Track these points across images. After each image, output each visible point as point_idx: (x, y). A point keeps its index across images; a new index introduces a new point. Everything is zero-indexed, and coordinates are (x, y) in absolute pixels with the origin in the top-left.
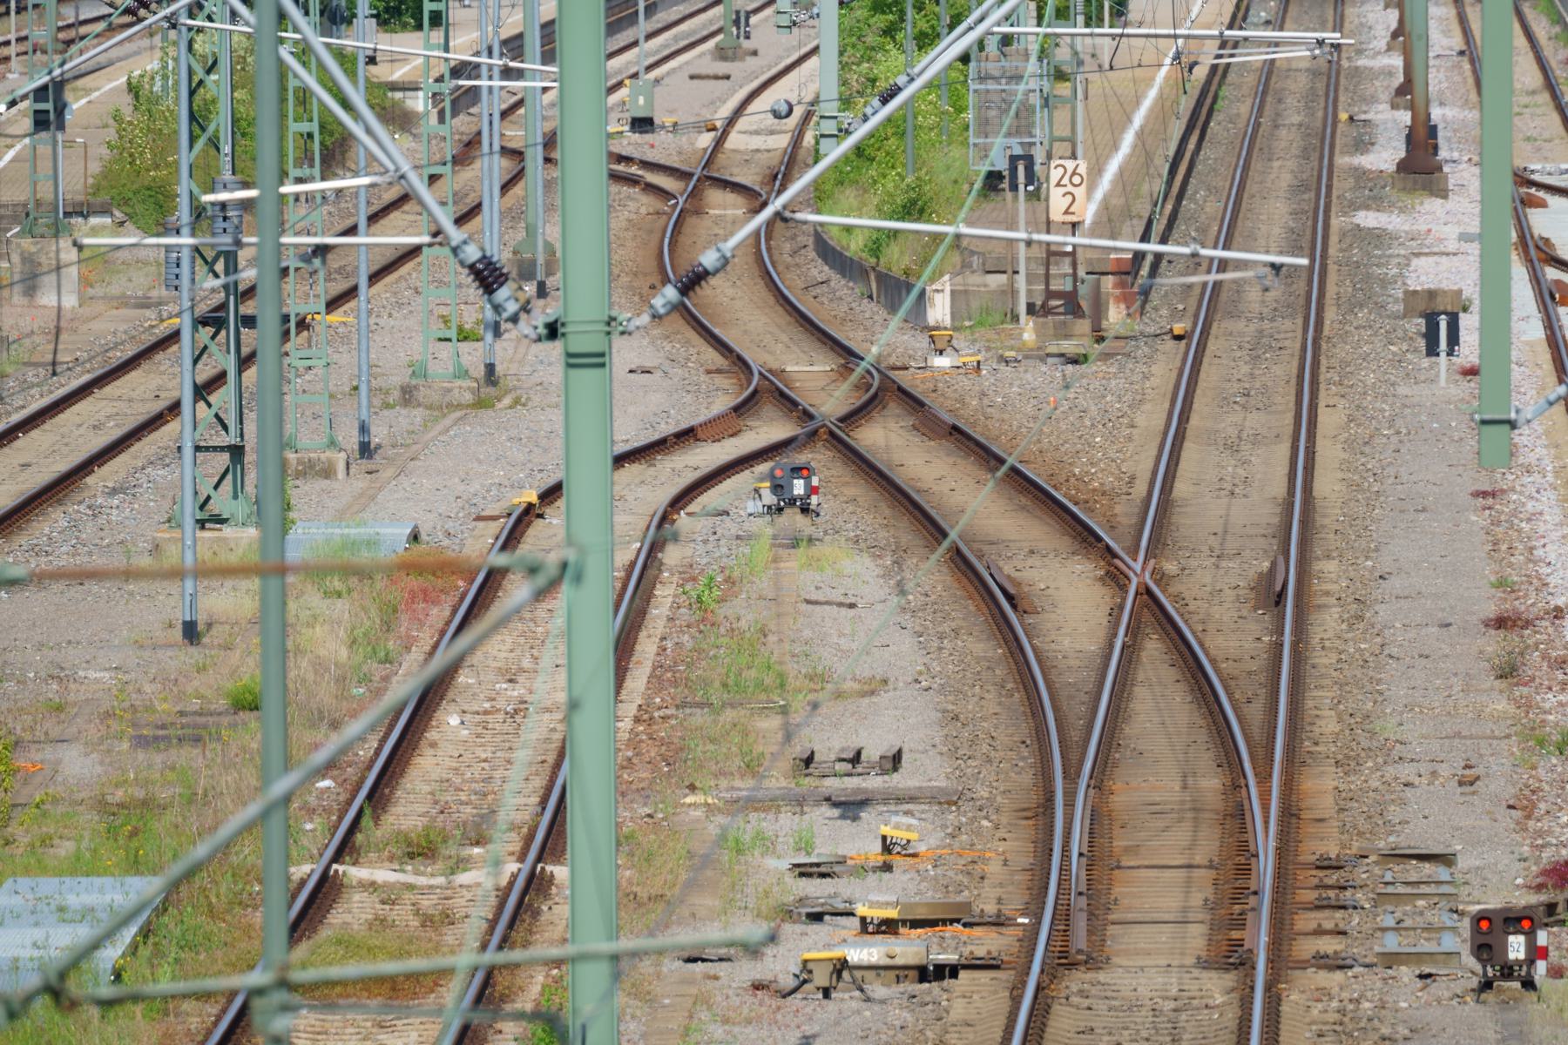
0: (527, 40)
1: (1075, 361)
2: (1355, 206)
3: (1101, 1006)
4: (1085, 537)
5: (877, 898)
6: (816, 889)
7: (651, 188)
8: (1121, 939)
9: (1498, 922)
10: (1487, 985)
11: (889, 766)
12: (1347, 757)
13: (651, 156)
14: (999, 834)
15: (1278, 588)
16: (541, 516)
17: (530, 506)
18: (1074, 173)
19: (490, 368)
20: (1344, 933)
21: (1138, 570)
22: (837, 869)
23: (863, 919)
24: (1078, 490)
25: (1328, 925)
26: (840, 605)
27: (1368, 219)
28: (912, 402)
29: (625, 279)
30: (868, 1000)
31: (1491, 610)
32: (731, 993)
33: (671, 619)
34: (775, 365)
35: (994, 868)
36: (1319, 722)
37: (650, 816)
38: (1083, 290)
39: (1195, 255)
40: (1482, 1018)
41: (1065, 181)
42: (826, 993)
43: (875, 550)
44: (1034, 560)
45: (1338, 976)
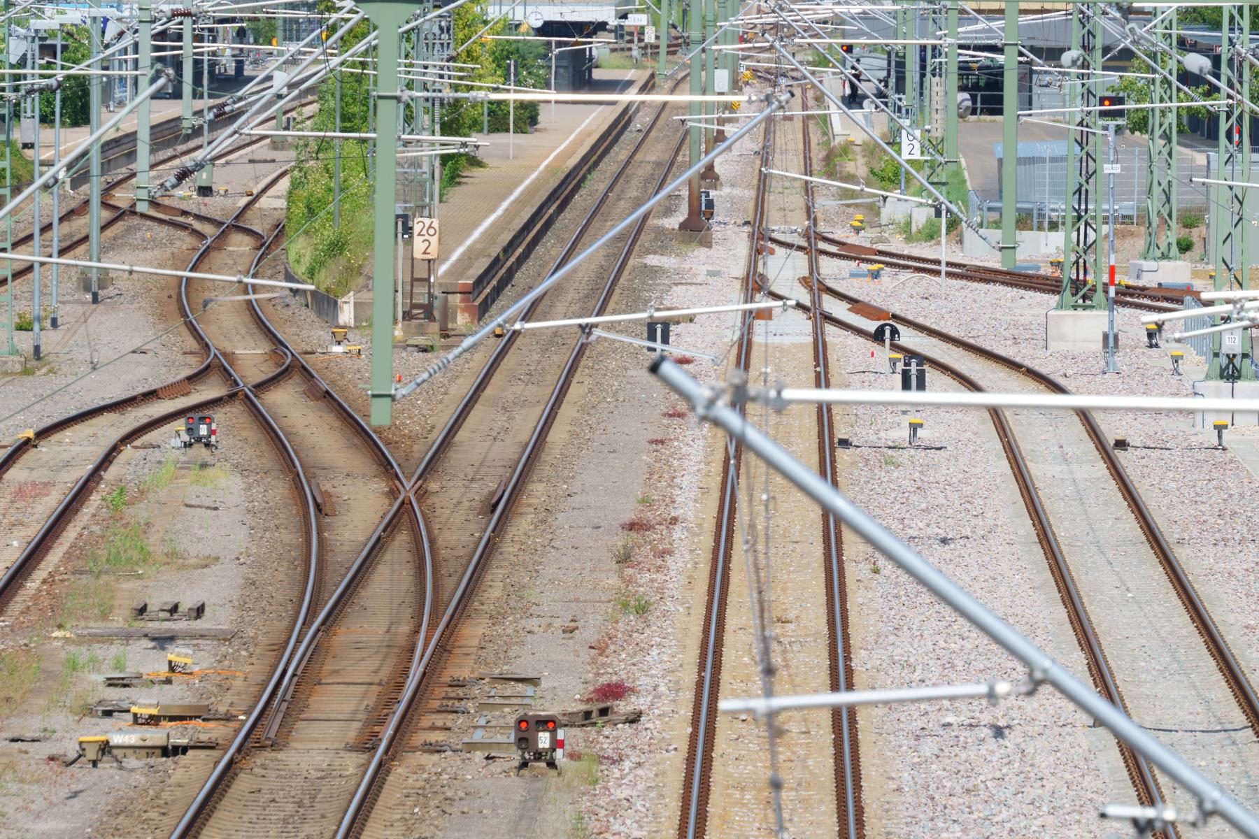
0: (139, 136)
1: (424, 350)
2: (648, 252)
3: (272, 774)
4: (385, 466)
5: (146, 702)
6: (115, 695)
7: (195, 232)
8: (304, 730)
9: (532, 723)
10: (524, 765)
11: (194, 614)
12: (499, 613)
13: (204, 212)
14: (251, 661)
15: (494, 501)
16: (35, 446)
17: (29, 440)
18: (430, 227)
19: (37, 349)
20: (449, 729)
21: (409, 487)
22: (134, 681)
23: (135, 715)
24: (394, 434)
25: (439, 723)
26: (208, 508)
27: (653, 260)
28: (307, 374)
29: (155, 291)
30: (121, 768)
31: (629, 517)
32: (32, 762)
33: (94, 515)
34: (229, 349)
35: (238, 683)
36: (489, 590)
37: (26, 645)
38: (437, 303)
39: (240, 282)
40: (517, 786)
41: (424, 232)
42: (95, 763)
43: (242, 470)
44: (349, 481)
45: (435, 757)
